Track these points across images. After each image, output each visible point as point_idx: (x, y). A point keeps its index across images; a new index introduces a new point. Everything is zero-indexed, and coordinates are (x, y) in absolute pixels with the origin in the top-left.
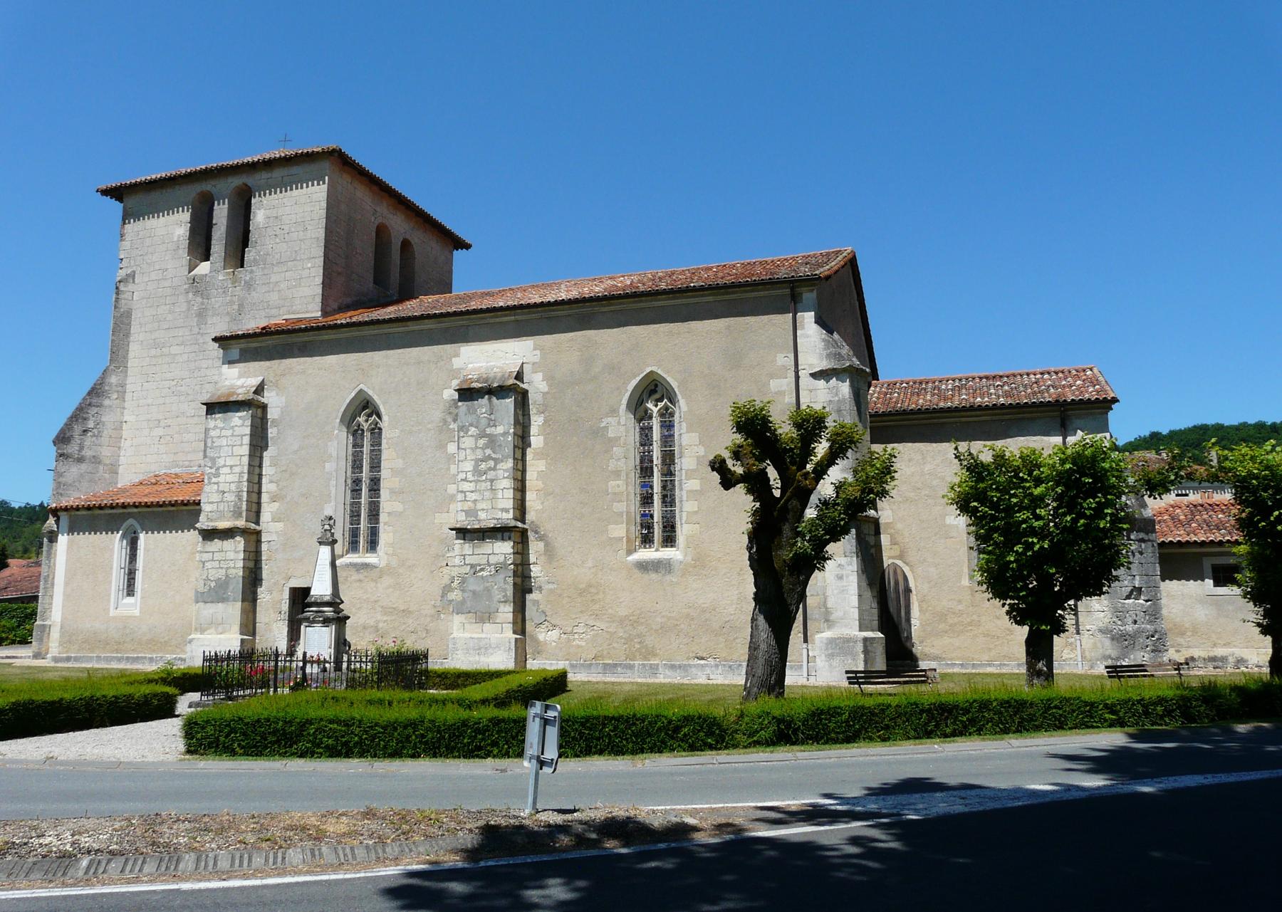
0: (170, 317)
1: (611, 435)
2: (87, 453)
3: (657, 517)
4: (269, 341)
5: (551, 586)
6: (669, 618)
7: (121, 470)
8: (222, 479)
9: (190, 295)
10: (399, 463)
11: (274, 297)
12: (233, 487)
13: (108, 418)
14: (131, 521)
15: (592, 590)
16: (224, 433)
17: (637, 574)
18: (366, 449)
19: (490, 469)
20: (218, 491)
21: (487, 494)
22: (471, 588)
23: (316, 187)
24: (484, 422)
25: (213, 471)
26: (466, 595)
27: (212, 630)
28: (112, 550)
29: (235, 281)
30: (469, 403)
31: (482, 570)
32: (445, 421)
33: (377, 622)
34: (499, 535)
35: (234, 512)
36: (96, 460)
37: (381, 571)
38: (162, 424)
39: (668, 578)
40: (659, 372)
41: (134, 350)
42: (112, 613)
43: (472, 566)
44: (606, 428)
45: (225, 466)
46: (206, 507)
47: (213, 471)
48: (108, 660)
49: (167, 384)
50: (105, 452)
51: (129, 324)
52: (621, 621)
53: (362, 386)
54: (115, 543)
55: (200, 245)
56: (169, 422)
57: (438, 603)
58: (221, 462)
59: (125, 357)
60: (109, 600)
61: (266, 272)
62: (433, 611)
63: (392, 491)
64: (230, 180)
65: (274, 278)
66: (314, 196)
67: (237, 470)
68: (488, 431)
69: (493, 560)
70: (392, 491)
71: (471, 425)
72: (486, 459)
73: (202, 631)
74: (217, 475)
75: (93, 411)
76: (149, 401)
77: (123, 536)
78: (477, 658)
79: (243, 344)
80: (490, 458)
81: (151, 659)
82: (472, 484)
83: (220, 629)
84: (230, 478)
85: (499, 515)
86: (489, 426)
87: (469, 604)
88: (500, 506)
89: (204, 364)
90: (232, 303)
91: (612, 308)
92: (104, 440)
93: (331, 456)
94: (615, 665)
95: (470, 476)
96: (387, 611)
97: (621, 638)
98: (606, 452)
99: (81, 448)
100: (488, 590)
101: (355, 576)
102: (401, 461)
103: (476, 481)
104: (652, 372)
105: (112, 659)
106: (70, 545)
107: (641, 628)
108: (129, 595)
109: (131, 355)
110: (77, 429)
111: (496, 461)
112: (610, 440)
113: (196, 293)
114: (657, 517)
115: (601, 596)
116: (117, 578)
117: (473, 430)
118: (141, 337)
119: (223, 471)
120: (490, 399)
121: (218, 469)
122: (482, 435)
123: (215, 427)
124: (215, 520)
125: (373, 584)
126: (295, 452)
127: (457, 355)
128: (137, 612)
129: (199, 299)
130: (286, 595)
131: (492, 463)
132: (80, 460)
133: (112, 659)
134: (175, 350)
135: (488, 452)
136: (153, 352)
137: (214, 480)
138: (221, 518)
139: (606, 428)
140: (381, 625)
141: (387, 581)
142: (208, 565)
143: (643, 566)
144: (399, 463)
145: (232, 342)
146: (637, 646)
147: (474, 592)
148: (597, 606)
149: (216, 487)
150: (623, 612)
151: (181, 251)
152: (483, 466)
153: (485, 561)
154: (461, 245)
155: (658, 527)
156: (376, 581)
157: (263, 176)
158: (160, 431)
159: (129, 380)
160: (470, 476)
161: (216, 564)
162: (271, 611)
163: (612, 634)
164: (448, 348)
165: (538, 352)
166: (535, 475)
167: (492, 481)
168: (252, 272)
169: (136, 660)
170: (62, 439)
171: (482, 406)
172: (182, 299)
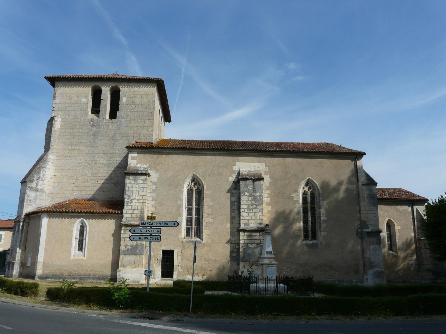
1: (295, 199)
2: (39, 187)
3: (310, 229)
8: (133, 204)
10: (211, 204)
11: (131, 132)
16: (134, 185)
19: (254, 208)
20: (131, 209)
24: (251, 191)
25: (129, 201)
27: (129, 267)
40: (312, 179)
44: (293, 197)
45: (135, 199)
47: (129, 201)
53: (194, 173)
56: (78, 178)
58: (133, 197)
63: (208, 214)
65: (131, 125)
67: (141, 201)
68: (253, 194)
70: (208, 214)
72: (252, 205)
74: (131, 202)
76: (68, 168)
80: (254, 204)
84: (137, 204)
86: (253, 193)
95: (246, 210)
99: (37, 185)
103: (249, 213)
104: (309, 179)
106: (49, 226)
108: (79, 250)
111: (257, 206)
112: (295, 201)
114: (310, 229)
116: (75, 243)
117: (247, 194)
119: (133, 201)
121: (132, 200)
123: (130, 183)
124: (130, 221)
128: (85, 258)
130: (161, 253)
131: (254, 206)
132: (37, 190)
134: (81, 148)
135: (253, 202)
136: (70, 148)
137: (129, 204)
138: (134, 220)
139: (293, 197)
140: (204, 266)
144: (211, 204)
149: (130, 207)
154: (360, 155)
155: (390, 225)
158: (74, 181)
160: (246, 210)
165: (267, 168)
166: (267, 212)
167: (255, 213)
170: (24, 182)
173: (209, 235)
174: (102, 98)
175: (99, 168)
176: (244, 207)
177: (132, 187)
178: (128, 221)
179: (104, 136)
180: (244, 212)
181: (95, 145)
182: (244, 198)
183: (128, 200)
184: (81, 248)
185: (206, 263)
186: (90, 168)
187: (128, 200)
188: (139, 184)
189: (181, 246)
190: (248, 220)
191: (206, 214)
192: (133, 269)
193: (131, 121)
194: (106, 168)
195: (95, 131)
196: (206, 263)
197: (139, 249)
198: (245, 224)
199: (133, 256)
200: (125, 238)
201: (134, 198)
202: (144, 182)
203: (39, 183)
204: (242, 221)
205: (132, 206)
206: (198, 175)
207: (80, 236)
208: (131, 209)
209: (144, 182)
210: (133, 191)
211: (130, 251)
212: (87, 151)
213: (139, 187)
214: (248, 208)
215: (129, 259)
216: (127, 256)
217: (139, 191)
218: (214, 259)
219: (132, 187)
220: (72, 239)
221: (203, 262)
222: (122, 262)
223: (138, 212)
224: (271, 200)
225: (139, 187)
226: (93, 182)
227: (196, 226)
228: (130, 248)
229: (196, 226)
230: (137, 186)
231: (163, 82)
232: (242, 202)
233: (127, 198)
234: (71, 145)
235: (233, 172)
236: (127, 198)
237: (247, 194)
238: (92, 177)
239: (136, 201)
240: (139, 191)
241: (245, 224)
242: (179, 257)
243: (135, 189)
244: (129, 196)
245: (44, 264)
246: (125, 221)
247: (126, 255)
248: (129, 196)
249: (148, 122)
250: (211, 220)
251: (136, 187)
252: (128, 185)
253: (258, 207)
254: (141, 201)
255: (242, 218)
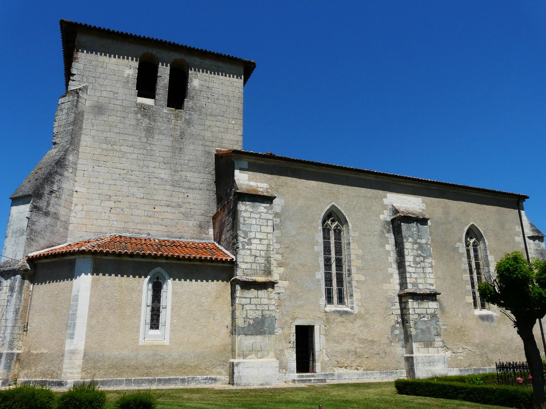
0: (120, 125)
2: (52, 209)
4: (272, 162)
5: (445, 327)
6: (496, 344)
7: (71, 227)
8: (253, 247)
9: (139, 116)
10: (360, 252)
11: (208, 134)
12: (263, 253)
13: (66, 185)
14: (159, 269)
15: (463, 329)
16: (253, 215)
17: (480, 321)
18: (332, 241)
19: (421, 261)
21: (422, 275)
22: (420, 327)
23: (228, 78)
24: (415, 236)
25: (246, 240)
26: (418, 331)
27: (253, 356)
28: (141, 291)
29: (177, 116)
30: (407, 224)
31: (424, 317)
32: (383, 232)
33: (356, 348)
34: (430, 298)
35: (265, 271)
36: (56, 216)
37: (356, 315)
38: (114, 198)
39: (492, 324)
41: (85, 141)
42: (141, 342)
43: (419, 315)
45: (255, 238)
46: (242, 266)
47: (246, 240)
48: (137, 382)
49: (118, 171)
50: (62, 211)
51: (82, 121)
52: (477, 346)
54: (144, 286)
55: (146, 85)
56: (120, 199)
57: (390, 337)
58: (252, 235)
59: (78, 144)
60: (138, 332)
61: (201, 117)
62: (388, 341)
63: (358, 269)
64: (172, 53)
65: (207, 123)
66: (235, 84)
67: (265, 242)
68: (418, 241)
69: (429, 311)
71: (409, 236)
73: (245, 356)
74: (250, 243)
75: (58, 177)
76: (101, 180)
77: (150, 281)
78: (429, 368)
79: (253, 160)
81: (183, 381)
82: (414, 269)
83: (260, 354)
84: (260, 247)
85: (429, 287)
86: (418, 238)
87: (420, 337)
88: (429, 282)
89: (152, 164)
90: (174, 129)
91: (455, 191)
92: (62, 202)
93: (317, 242)
94: (167, 405)
96: (363, 341)
97: (478, 354)
98: (460, 259)
100: (428, 328)
101: (340, 319)
102: (361, 251)
103: (416, 267)
104: (473, 224)
105: (143, 381)
107: (486, 350)
108: (152, 328)
109: (83, 143)
110: (47, 189)
113: (144, 115)
115: (467, 333)
116: (146, 314)
118: (93, 133)
119: (253, 241)
120: (417, 224)
121: (250, 240)
122: (415, 243)
123: (246, 211)
124: (251, 275)
125: (351, 324)
126: (294, 236)
127: (386, 197)
128: (167, 342)
129: (147, 120)
130: (294, 330)
132: (47, 214)
133: (143, 381)
135: (420, 252)
136: (104, 146)
137: (247, 247)
140: (358, 350)
141: (359, 322)
142: (247, 307)
143: (483, 318)
144: (360, 252)
145: (245, 156)
146: (485, 359)
147: (422, 329)
148: (466, 338)
149: (249, 252)
150: (477, 341)
151: (130, 85)
152: (418, 259)
153: (424, 312)
156: (352, 322)
157: (197, 60)
158: (112, 204)
159: (80, 161)
161: (253, 307)
162: (284, 341)
163: (474, 353)
164: (381, 192)
165: (424, 204)
167: (423, 268)
168: (190, 114)
169: (168, 381)
171: (414, 227)
172: (131, 116)
173: (360, 300)
174: (159, 75)
175: (156, 187)
176: (409, 259)
177: (249, 218)
178: (247, 275)
179: (164, 134)
180: (410, 266)
181: (149, 148)
182: (408, 245)
183: (243, 240)
184: (155, 323)
185: (361, 346)
186: (140, 185)
187: (243, 240)
188: (260, 213)
189: (324, 318)
190: (416, 278)
191: (355, 268)
192: (260, 360)
193: (208, 118)
194: (168, 187)
195: (150, 124)
196: (361, 346)
197: (267, 324)
198: (414, 284)
199: (259, 337)
200: (243, 305)
201: (254, 236)
202: (268, 210)
203: (52, 202)
204: (408, 280)
205: (250, 249)
206: (339, 208)
207: (153, 302)
208: (251, 255)
209: (268, 210)
210: (251, 224)
211: (252, 329)
212: (135, 156)
213: (260, 218)
214: (415, 262)
215: (251, 342)
216: (249, 337)
217: (261, 225)
218: (370, 339)
219: (249, 218)
220: (140, 305)
221: (357, 345)
222: (239, 347)
223: (262, 260)
224: (125, 274)
225: (260, 218)
226: (146, 208)
227: (336, 286)
228: (251, 322)
229: (336, 286)
230: (257, 216)
231: (255, 66)
232: (406, 252)
233: (243, 235)
234: (106, 141)
235: (385, 207)
236: (243, 235)
237: (410, 239)
238: (145, 201)
239: (257, 241)
240: (261, 225)
241: (414, 284)
242: (323, 337)
243: (254, 222)
244: (246, 233)
245: (85, 355)
246: (241, 274)
247: (246, 335)
248: (246, 233)
249: (233, 122)
250: (363, 278)
251: (256, 219)
252: (244, 214)
253: (426, 260)
254: (265, 242)
255: (408, 275)
